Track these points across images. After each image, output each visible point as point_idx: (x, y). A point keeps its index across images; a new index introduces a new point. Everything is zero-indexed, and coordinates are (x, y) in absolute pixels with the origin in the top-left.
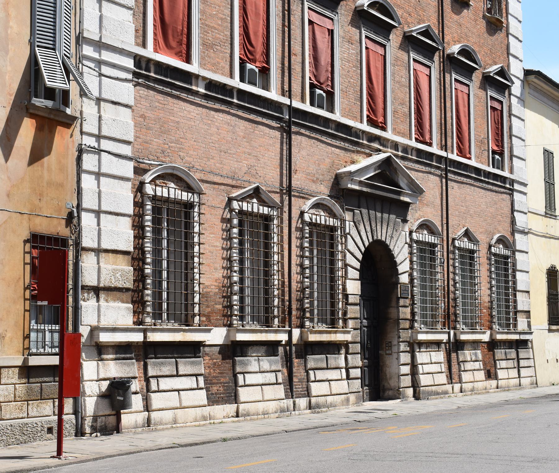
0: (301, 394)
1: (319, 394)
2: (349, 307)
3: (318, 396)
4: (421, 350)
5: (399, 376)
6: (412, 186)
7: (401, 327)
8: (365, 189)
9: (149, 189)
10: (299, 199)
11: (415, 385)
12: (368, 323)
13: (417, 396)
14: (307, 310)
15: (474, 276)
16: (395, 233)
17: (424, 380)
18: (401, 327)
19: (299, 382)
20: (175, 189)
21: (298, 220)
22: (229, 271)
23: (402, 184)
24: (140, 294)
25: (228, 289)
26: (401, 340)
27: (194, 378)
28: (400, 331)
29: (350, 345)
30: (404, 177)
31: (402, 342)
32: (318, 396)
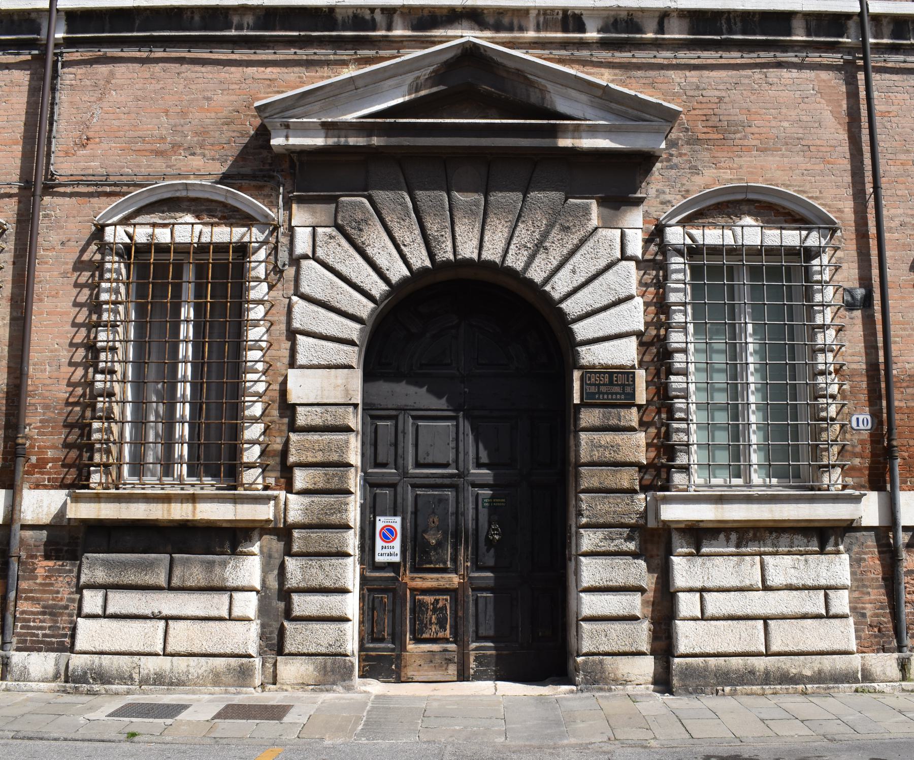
0: (42, 642)
1: (106, 648)
2: (294, 437)
3: (102, 653)
4: (704, 550)
5: (578, 621)
6: (614, 106)
7: (584, 484)
8: (375, 141)
9: (675, 235)
10: (92, 200)
11: (664, 645)
12: (495, 476)
13: (663, 682)
14: (98, 446)
15: (814, 327)
16: (555, 234)
17: (689, 636)
18: (584, 484)
19: (44, 613)
20: (193, 224)
21: (88, 244)
22: (91, 370)
23: (562, 106)
24: (663, 429)
25: (84, 412)
26: (584, 520)
27: (698, 595)
28: (582, 496)
29: (296, 533)
30: (567, 86)
31: (587, 526)
32: (102, 653)
